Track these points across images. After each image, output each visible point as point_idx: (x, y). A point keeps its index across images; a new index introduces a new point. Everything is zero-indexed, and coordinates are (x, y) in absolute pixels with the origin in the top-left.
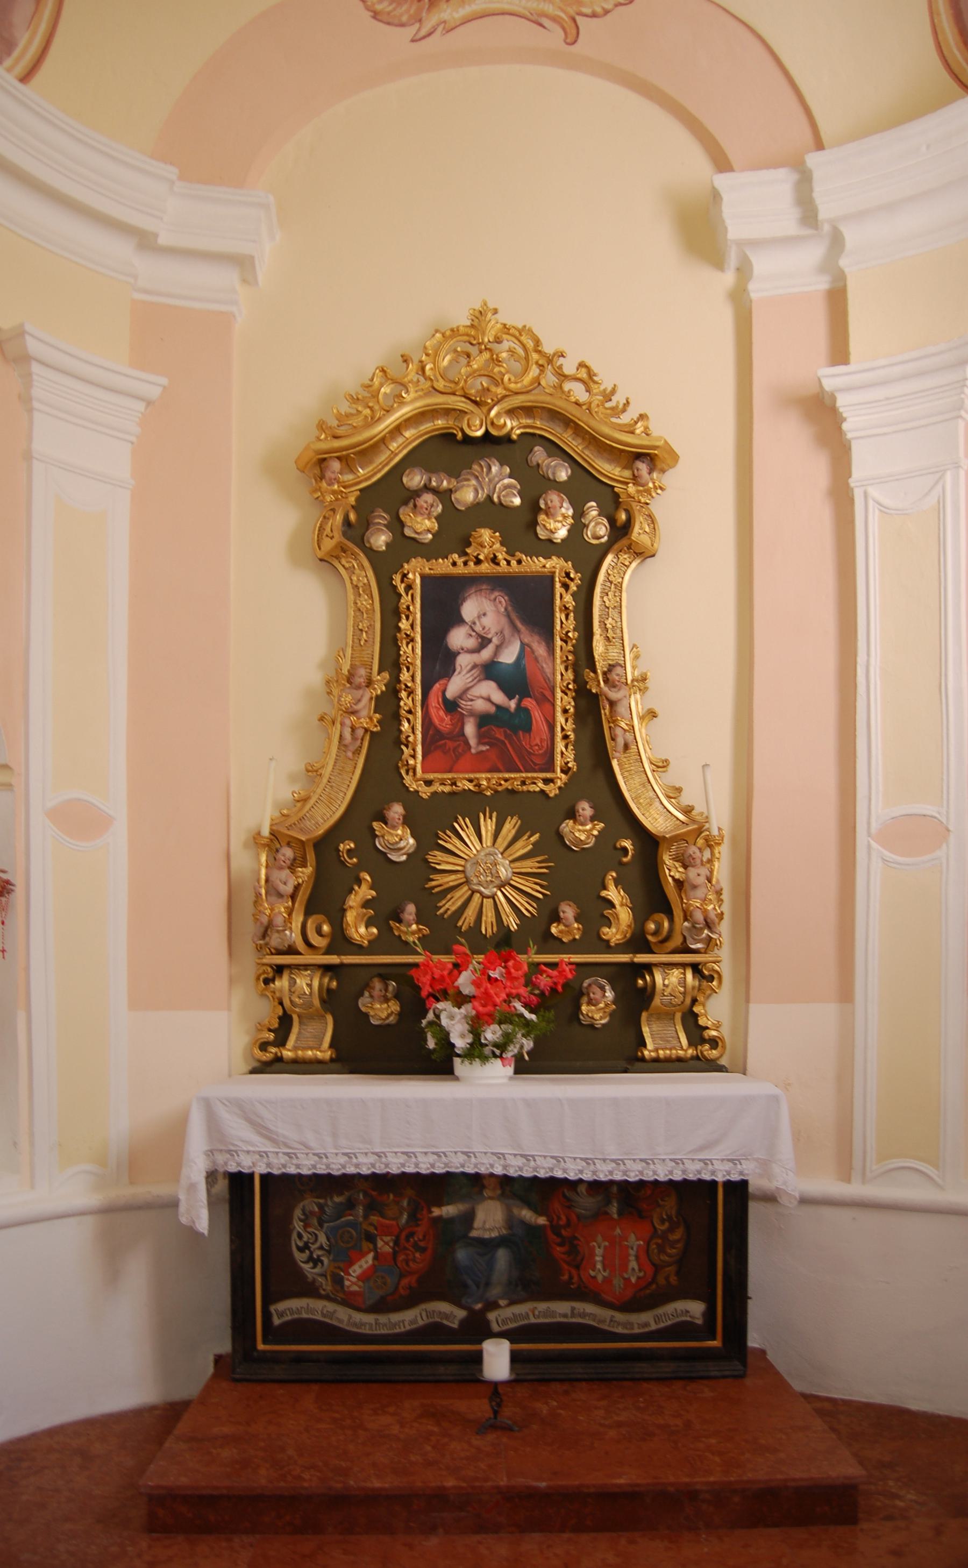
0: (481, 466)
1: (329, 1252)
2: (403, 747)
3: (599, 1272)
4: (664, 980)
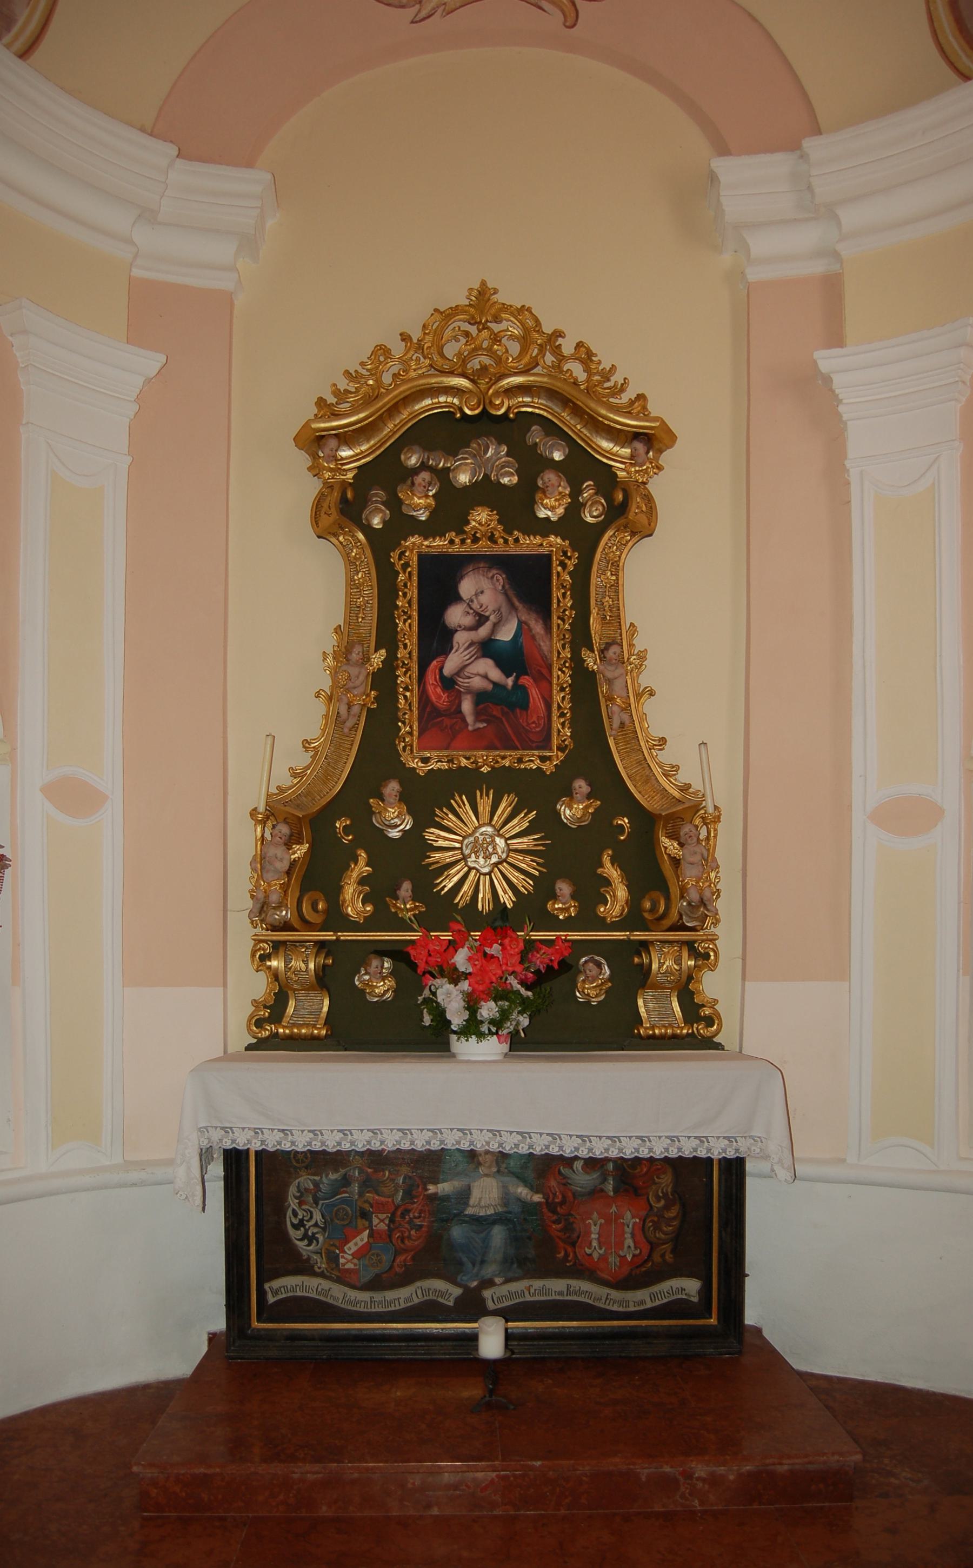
1: (324, 1229)
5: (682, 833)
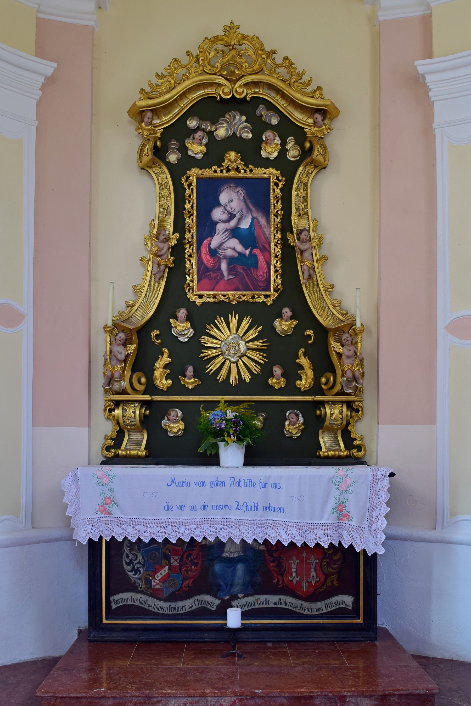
1: (143, 565)
2: (187, 276)
3: (294, 578)
5: (343, 339)
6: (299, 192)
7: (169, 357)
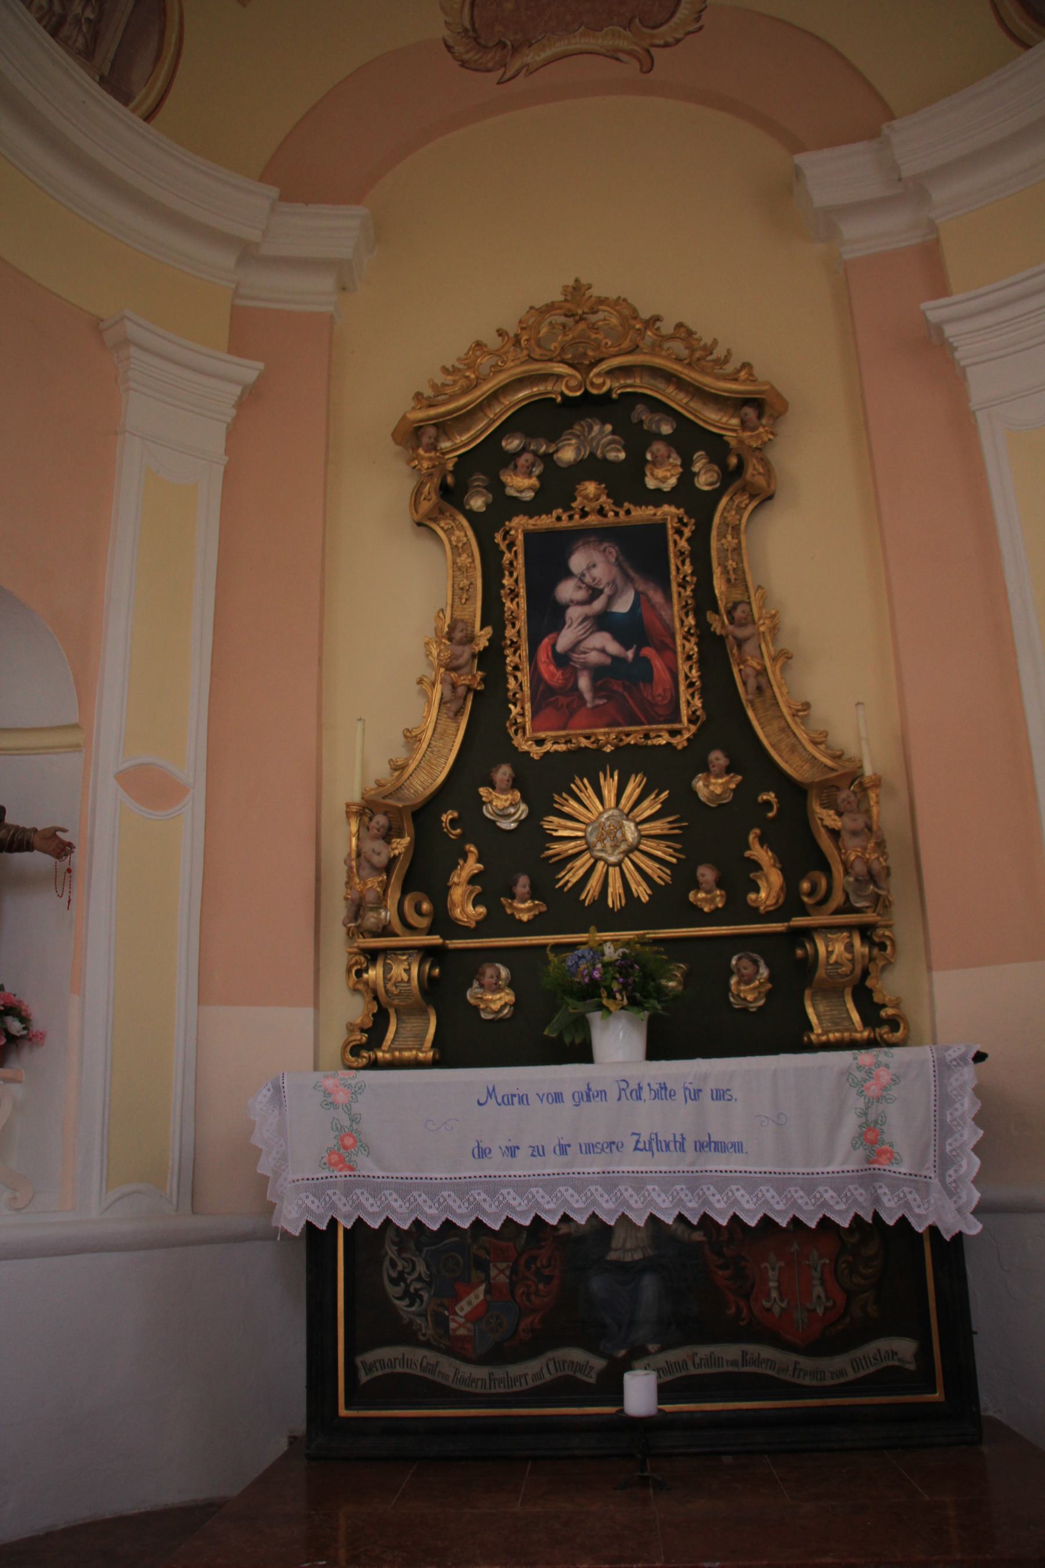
0: (582, 426)
1: (429, 1284)
2: (511, 706)
3: (774, 1302)
4: (827, 947)
5: (839, 801)
6: (723, 541)
7: (479, 861)
